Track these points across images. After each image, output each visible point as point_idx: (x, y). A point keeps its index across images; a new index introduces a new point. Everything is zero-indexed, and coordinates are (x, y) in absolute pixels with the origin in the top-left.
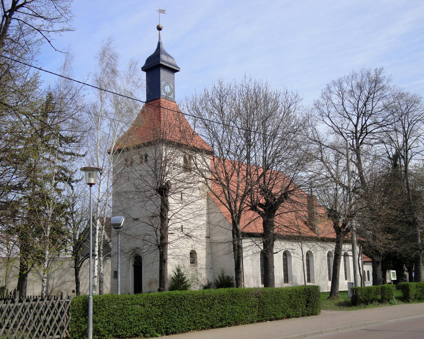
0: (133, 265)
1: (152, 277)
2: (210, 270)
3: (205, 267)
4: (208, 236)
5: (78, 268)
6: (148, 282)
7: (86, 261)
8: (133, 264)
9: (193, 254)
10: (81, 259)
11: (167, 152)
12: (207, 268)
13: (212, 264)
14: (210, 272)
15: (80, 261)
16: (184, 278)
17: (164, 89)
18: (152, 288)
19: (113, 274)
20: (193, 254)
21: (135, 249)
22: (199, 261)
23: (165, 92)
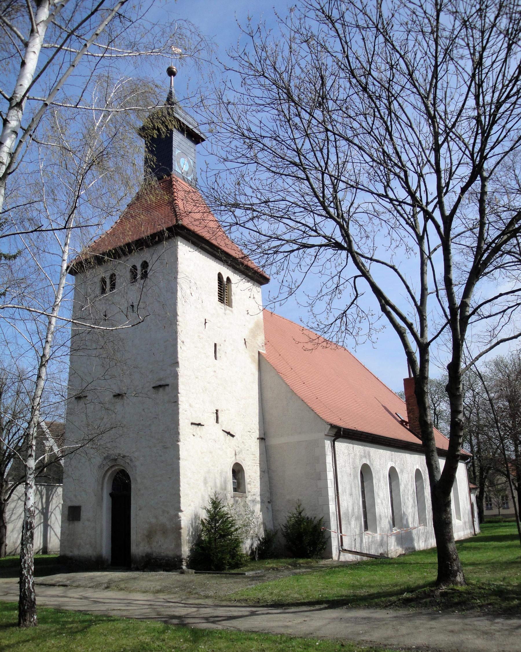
0: (111, 495)
1: (153, 521)
2: (267, 504)
3: (258, 499)
4: (262, 436)
5: (5, 500)
6: (145, 532)
7: (21, 488)
8: (110, 491)
9: (238, 471)
10: (10, 485)
11: (187, 256)
12: (262, 502)
13: (271, 493)
14: (267, 508)
15: (9, 489)
16: (308, 518)
17: (179, 162)
18: (155, 544)
19: (66, 513)
20: (238, 471)
21: (116, 460)
22: (248, 487)
23: (180, 167)
